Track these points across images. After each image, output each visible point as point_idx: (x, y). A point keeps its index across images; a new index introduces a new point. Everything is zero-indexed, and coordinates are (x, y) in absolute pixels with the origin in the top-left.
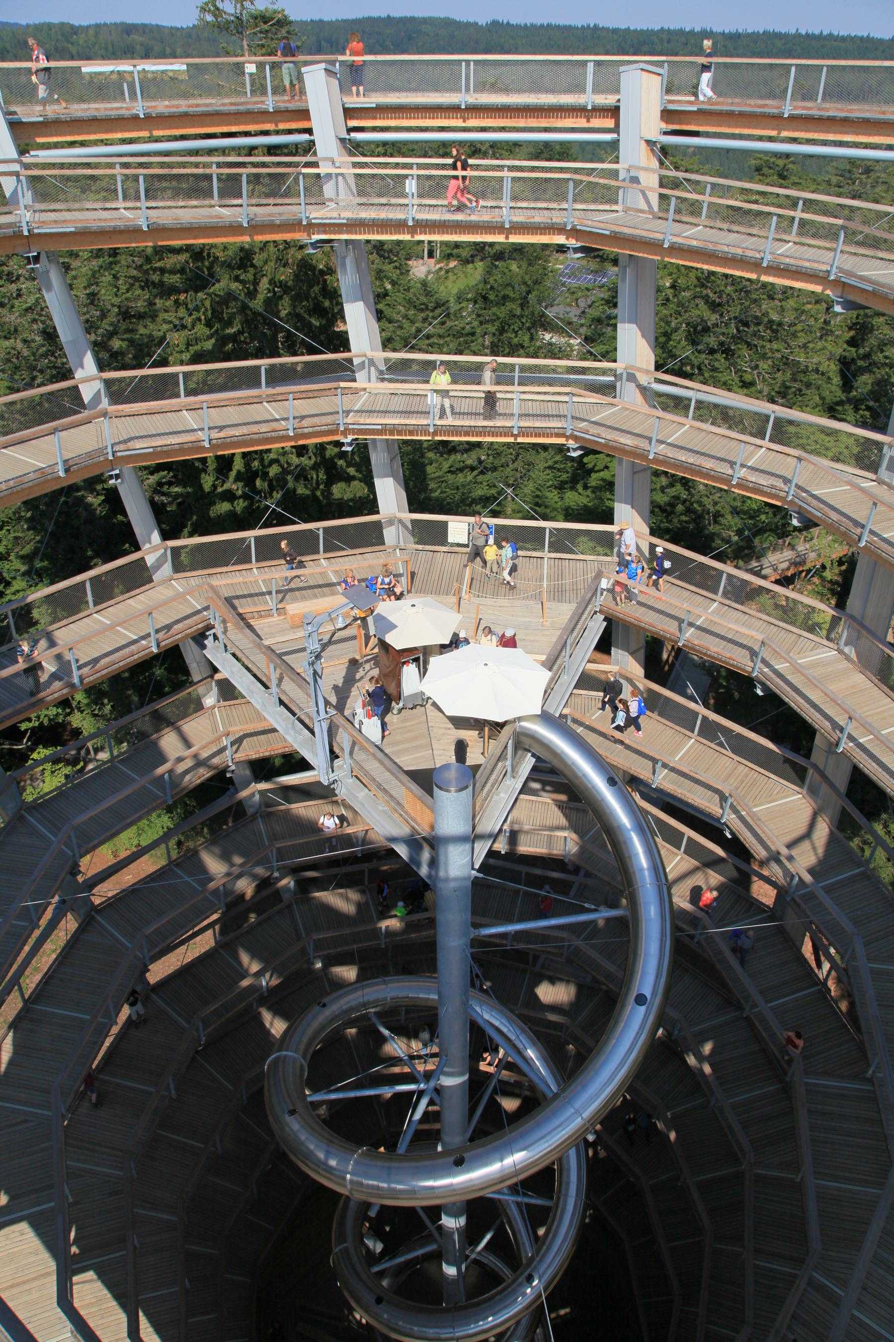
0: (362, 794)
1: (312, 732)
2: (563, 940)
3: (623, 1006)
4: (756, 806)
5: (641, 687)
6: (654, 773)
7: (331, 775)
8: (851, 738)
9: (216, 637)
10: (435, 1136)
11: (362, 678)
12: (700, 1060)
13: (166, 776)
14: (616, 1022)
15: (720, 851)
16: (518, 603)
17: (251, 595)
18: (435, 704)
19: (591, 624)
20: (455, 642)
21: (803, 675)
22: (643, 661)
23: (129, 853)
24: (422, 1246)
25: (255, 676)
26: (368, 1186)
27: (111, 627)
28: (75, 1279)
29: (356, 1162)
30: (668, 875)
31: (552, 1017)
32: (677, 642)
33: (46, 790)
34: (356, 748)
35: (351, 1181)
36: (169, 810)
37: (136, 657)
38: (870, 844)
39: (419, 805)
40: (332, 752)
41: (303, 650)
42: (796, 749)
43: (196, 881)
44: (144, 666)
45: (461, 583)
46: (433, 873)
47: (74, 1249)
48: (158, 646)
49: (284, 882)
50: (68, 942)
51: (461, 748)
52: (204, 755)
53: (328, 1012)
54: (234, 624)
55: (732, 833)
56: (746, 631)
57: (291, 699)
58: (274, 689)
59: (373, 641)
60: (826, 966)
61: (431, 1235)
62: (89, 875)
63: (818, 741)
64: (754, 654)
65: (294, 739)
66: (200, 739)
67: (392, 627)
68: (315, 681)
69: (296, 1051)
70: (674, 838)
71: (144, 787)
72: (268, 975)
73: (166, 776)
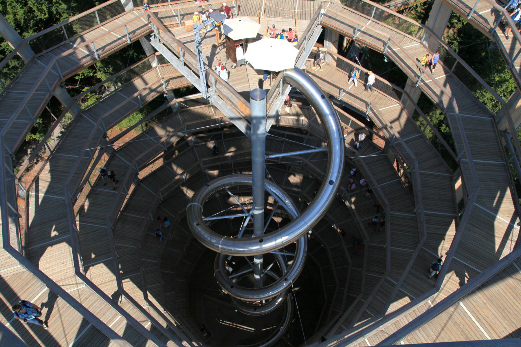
0: (221, 102)
1: (199, 77)
2: (300, 160)
3: (324, 185)
4: (380, 108)
5: (336, 58)
6: (340, 94)
7: (208, 95)
8: (422, 81)
9: (155, 36)
10: (252, 232)
11: (219, 53)
12: (351, 204)
13: (139, 97)
14: (321, 191)
15: (363, 125)
16: (285, 20)
17: (169, 17)
18: (250, 64)
19: (316, 30)
20: (259, 37)
21: (405, 53)
22: (337, 46)
23: (126, 129)
24: (247, 269)
25: (173, 53)
26: (228, 250)
27: (109, 32)
28: (123, 281)
29: (222, 241)
30: (341, 135)
31: (295, 189)
32: (352, 38)
33: (89, 104)
34: (217, 83)
35: (222, 248)
36: (141, 111)
37: (121, 45)
38: (424, 125)
39: (244, 106)
40: (207, 85)
41: (194, 41)
42: (398, 85)
43: (155, 139)
44: (125, 49)
45: (260, 11)
46: (248, 132)
47: (121, 272)
48: (130, 40)
49: (190, 138)
50: (106, 164)
51: (261, 83)
52: (154, 87)
53: (210, 188)
54: (162, 30)
55: (370, 119)
56: (382, 34)
57: (189, 63)
58: (182, 58)
59: (223, 37)
60: (402, 171)
61: (250, 266)
62: (111, 138)
63: (408, 82)
64: (385, 44)
65: (191, 80)
66: (152, 80)
67: (231, 30)
68: (199, 54)
69: (198, 203)
70: (347, 121)
71: (130, 101)
72: (185, 175)
73: (139, 97)
